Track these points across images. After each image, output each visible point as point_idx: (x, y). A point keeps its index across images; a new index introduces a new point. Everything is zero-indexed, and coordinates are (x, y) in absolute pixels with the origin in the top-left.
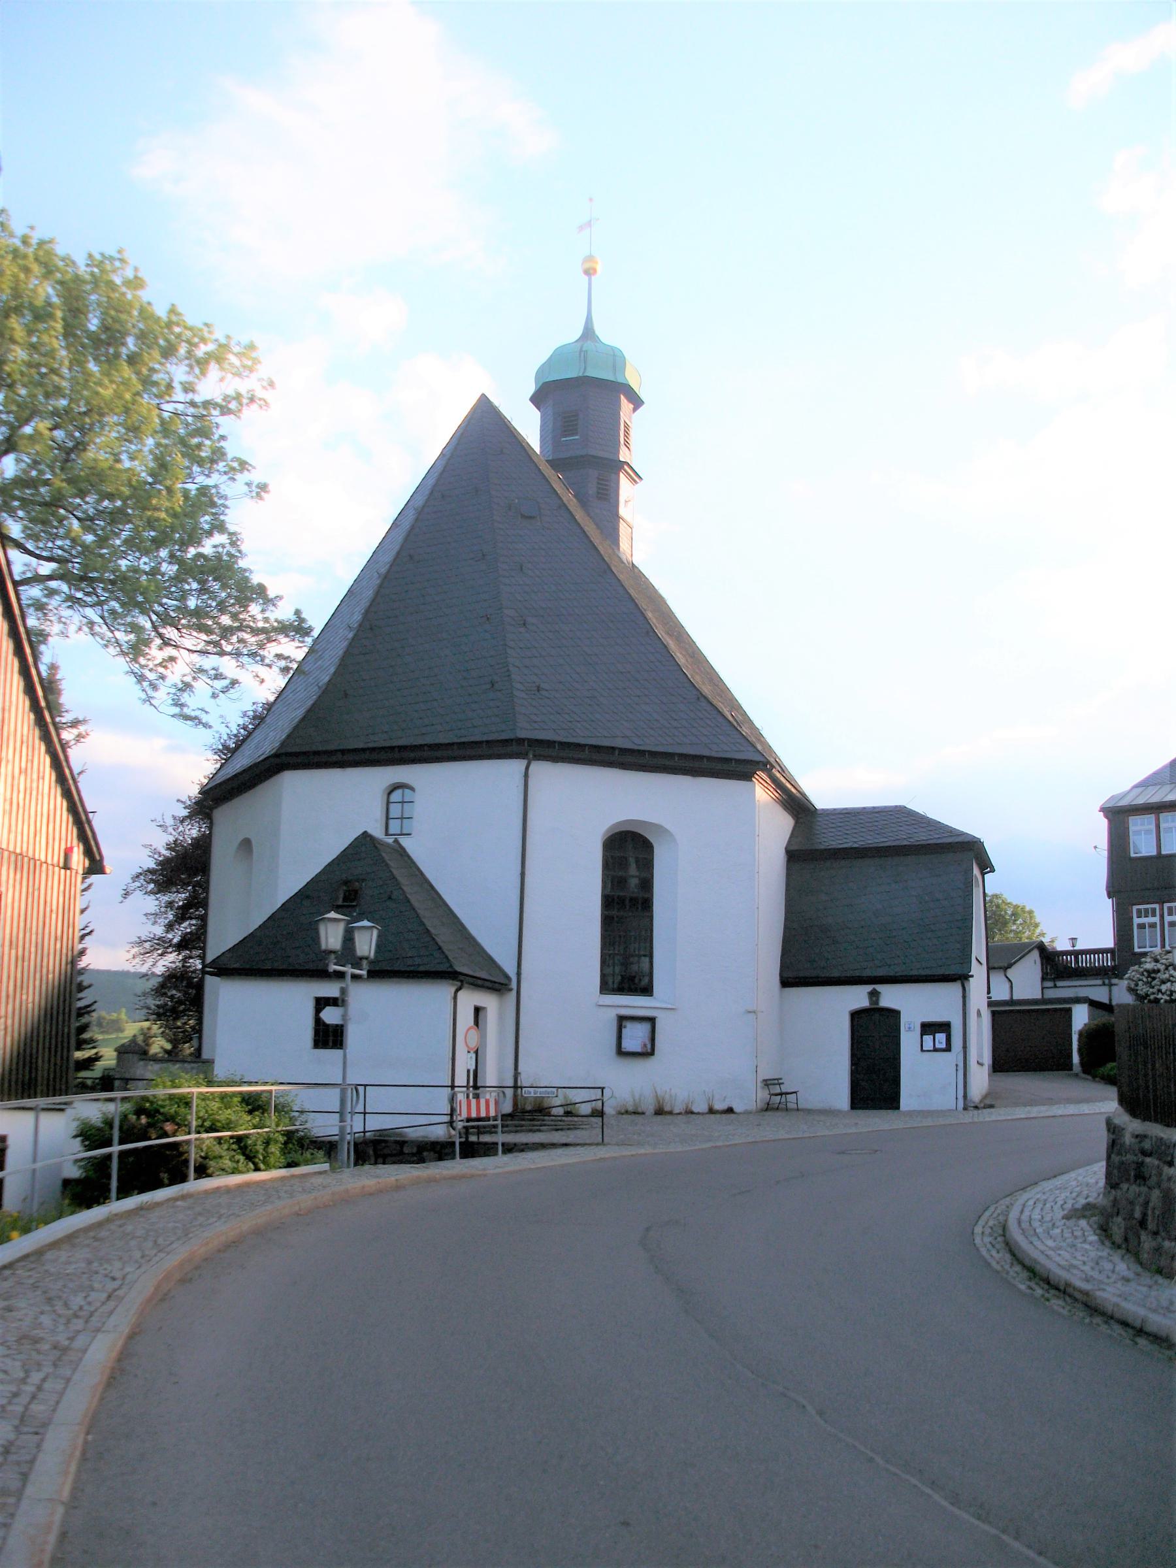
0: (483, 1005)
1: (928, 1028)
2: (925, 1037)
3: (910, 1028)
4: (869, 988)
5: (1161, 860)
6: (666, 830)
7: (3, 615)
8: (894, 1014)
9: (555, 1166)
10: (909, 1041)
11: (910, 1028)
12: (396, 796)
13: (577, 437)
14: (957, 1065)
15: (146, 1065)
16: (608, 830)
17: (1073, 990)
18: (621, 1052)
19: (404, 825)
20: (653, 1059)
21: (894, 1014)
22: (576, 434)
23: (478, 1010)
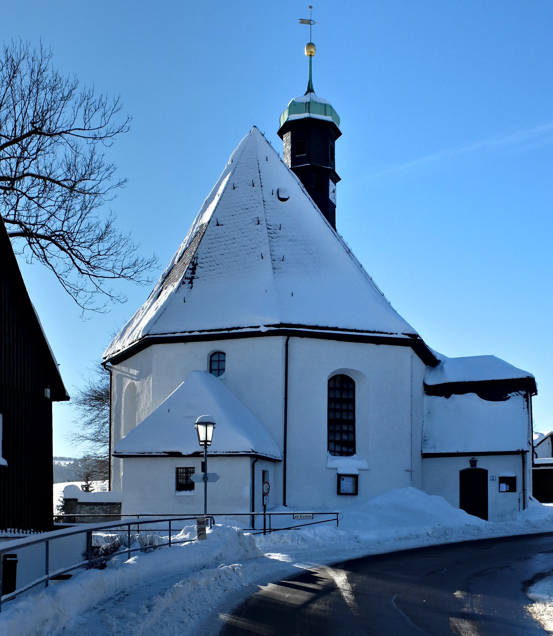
0: (268, 470)
1: (503, 480)
2: (501, 484)
3: (493, 479)
4: (470, 458)
5: (2, 181)
6: (356, 371)
7: (334, 206)
8: (485, 472)
9: (312, 562)
10: (493, 487)
11: (493, 479)
12: (215, 358)
13: (305, 155)
14: (519, 499)
15: (81, 507)
16: (331, 374)
17: (182, 249)
18: (339, 493)
19: (218, 367)
20: (357, 497)
21: (485, 472)
22: (304, 154)
23: (264, 472)
